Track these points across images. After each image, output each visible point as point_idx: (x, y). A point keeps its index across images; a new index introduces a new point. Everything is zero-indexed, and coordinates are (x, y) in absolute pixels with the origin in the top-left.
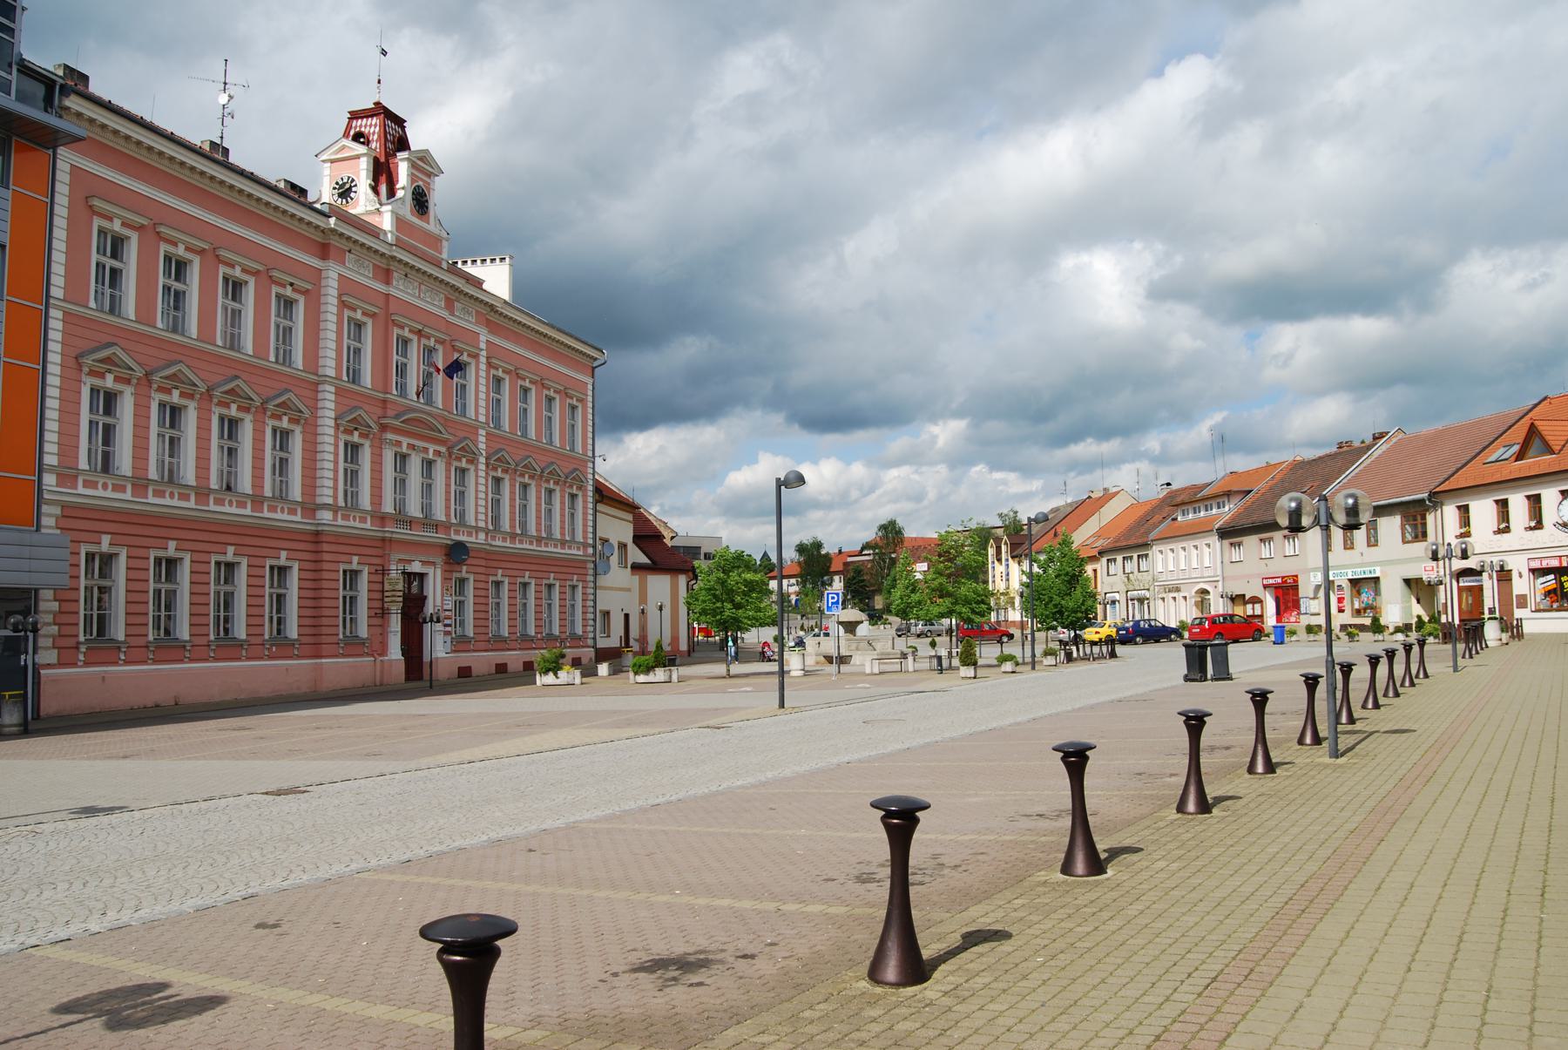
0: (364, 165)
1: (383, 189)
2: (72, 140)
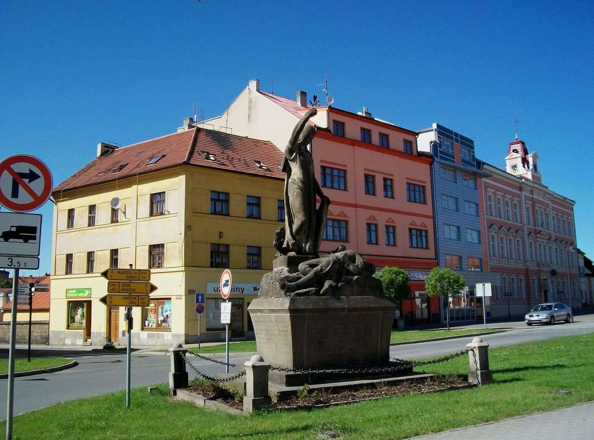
0: (520, 160)
1: (526, 166)
2: (486, 176)
